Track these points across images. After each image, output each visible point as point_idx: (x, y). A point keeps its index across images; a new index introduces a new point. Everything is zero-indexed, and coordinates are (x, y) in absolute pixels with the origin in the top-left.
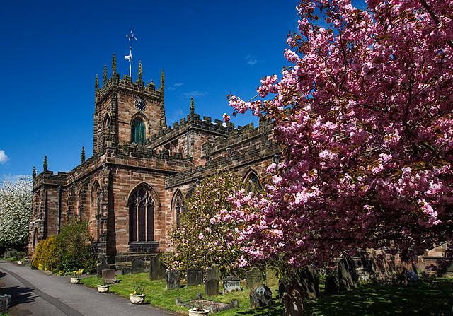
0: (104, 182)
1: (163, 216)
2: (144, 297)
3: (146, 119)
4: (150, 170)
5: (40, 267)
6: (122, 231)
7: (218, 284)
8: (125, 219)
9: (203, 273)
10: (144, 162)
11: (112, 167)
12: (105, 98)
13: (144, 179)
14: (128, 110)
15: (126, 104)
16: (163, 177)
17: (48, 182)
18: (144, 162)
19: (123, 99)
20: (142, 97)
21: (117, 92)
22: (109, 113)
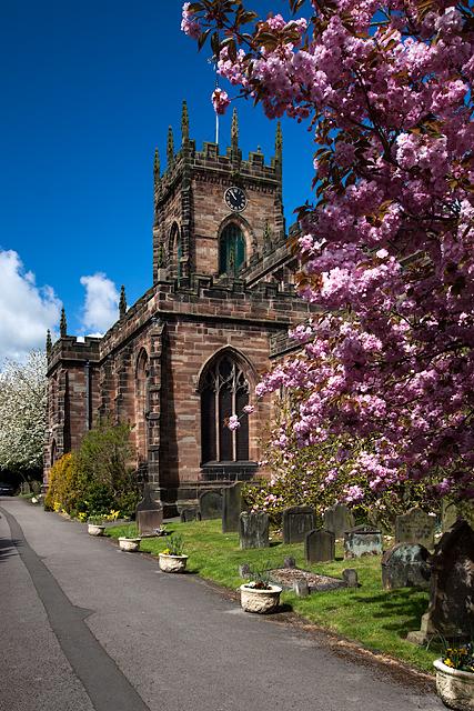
0: (153, 348)
1: (265, 411)
2: (184, 560)
3: (247, 226)
4: (240, 323)
5: (57, 505)
6: (189, 441)
7: (332, 541)
8: (193, 417)
9: (315, 519)
10: (229, 306)
11: (168, 319)
12: (171, 191)
14: (213, 211)
15: (209, 200)
16: (265, 334)
17: (70, 355)
18: (229, 306)
19: (202, 190)
20: (238, 182)
21: (186, 181)
22: (178, 220)
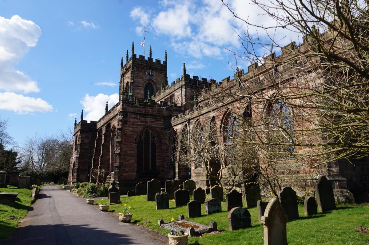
10: (149, 109)
13: (149, 122)
16: (163, 120)
18: (149, 109)
19: (138, 70)
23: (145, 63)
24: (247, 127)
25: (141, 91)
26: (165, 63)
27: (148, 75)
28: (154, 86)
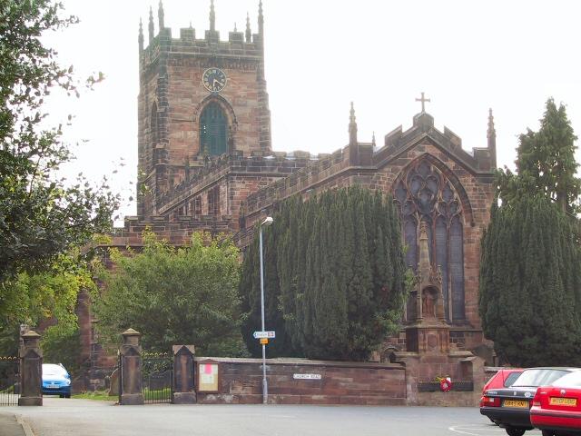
23: (197, 51)
24: (189, 311)
25: (189, 133)
26: (259, 38)
27: (207, 84)
28: (227, 112)
